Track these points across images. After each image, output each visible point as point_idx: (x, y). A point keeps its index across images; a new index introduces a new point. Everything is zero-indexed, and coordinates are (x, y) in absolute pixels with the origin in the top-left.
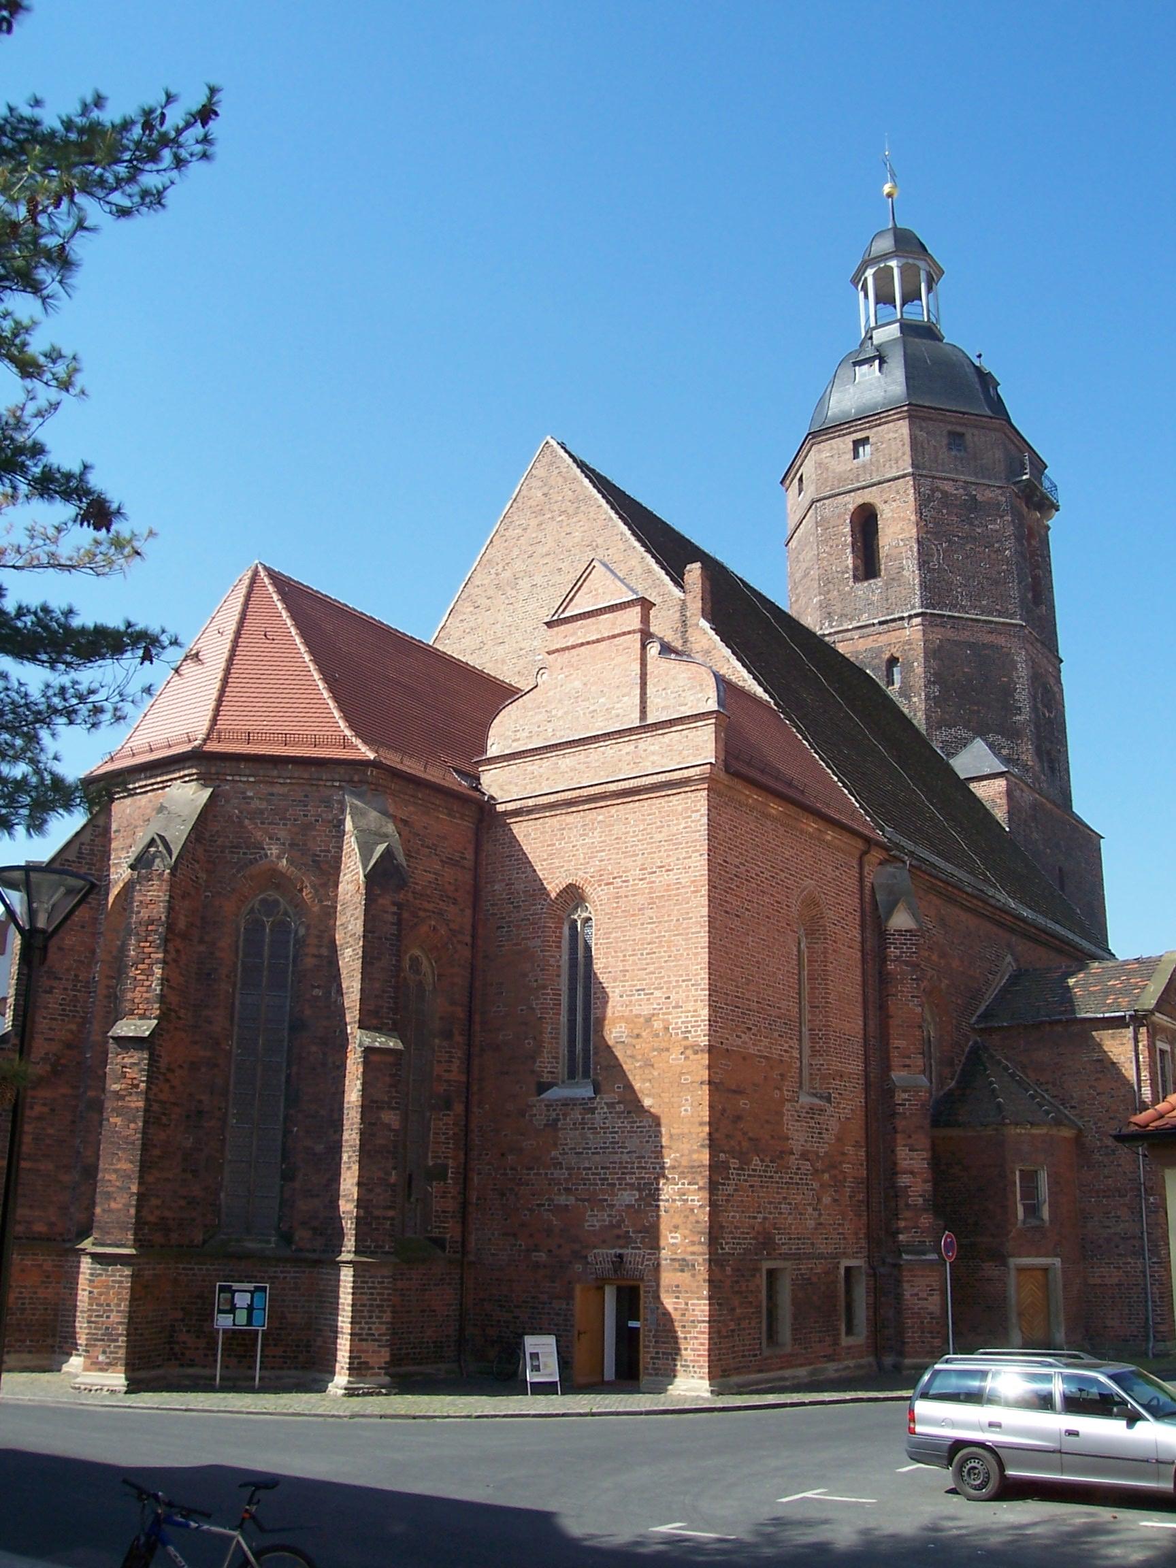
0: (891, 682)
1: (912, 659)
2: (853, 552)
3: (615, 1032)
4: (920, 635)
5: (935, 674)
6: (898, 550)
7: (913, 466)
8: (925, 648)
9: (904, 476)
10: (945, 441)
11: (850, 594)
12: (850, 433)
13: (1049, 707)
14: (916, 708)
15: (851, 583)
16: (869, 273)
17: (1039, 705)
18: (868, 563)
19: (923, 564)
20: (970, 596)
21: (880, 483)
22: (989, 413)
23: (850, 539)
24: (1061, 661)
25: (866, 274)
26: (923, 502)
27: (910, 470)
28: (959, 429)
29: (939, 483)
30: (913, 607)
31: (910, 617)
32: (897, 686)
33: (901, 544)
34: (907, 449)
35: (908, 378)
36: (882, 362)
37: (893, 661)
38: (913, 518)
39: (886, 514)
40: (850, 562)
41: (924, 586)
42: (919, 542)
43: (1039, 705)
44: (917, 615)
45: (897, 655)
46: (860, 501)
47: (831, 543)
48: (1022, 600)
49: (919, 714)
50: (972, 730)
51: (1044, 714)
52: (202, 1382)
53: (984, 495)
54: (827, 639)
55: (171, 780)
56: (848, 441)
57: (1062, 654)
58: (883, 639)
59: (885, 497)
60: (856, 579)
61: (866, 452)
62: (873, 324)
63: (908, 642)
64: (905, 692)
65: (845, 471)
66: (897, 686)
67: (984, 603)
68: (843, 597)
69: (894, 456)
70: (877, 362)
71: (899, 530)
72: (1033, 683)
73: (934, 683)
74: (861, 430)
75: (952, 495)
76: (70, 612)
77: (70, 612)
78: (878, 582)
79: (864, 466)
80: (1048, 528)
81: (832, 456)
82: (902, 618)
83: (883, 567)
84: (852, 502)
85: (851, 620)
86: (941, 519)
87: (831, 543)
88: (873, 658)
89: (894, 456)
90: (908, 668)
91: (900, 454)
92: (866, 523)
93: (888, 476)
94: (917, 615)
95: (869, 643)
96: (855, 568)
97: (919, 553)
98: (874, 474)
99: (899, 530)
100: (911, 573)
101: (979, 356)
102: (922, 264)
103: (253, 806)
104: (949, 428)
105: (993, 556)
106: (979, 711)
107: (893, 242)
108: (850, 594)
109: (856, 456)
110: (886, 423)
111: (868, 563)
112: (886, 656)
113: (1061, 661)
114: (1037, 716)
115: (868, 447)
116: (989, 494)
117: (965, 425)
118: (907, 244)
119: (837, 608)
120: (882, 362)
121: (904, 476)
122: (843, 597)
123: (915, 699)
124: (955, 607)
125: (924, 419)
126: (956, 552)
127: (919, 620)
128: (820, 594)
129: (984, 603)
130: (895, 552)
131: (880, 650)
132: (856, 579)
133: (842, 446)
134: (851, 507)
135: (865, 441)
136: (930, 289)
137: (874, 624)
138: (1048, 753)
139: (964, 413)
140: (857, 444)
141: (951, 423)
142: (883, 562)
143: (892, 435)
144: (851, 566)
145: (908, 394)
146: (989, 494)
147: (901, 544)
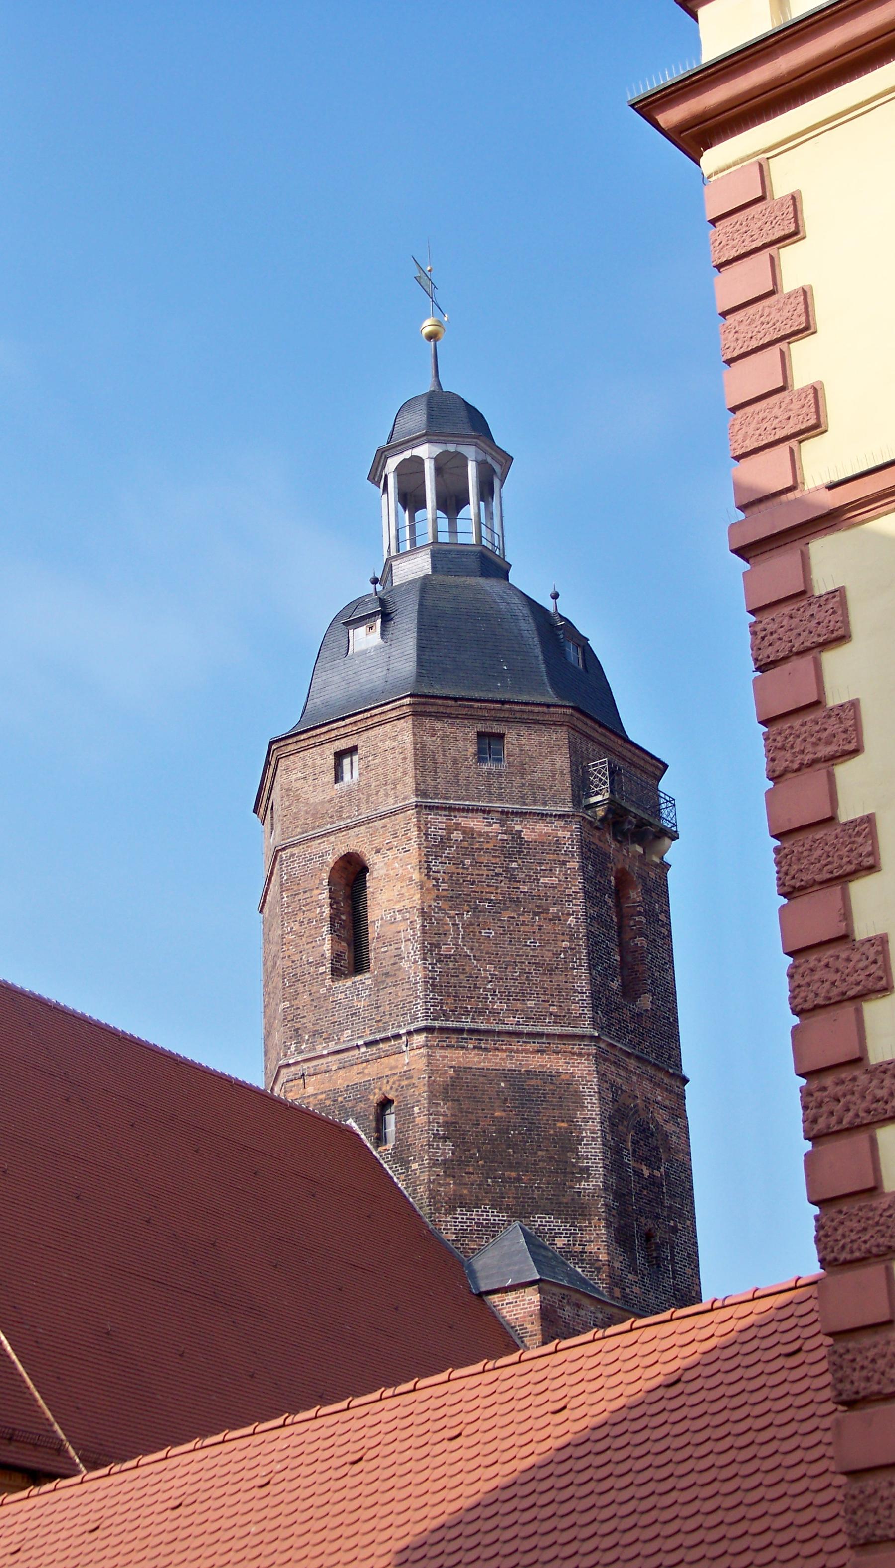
0: (380, 1139)
1: (411, 1101)
2: (333, 930)
4: (421, 1064)
5: (446, 1124)
6: (394, 928)
7: (419, 792)
8: (430, 1085)
9: (404, 809)
10: (472, 749)
11: (326, 998)
12: (330, 740)
13: (653, 1161)
14: (416, 1180)
15: (328, 982)
16: (392, 463)
17: (629, 1160)
19: (431, 948)
20: (508, 996)
21: (370, 820)
22: (555, 700)
23: (327, 911)
24: (685, 1081)
25: (386, 471)
26: (434, 848)
27: (413, 799)
28: (496, 728)
30: (414, 1019)
31: (409, 1033)
32: (390, 1146)
33: (399, 917)
34: (410, 766)
35: (421, 648)
36: (386, 617)
37: (385, 1104)
38: (416, 876)
41: (432, 984)
42: (423, 914)
43: (629, 1160)
44: (418, 1031)
45: (390, 1096)
46: (342, 850)
47: (300, 917)
48: (595, 996)
49: (421, 1189)
50: (508, 1209)
51: (639, 1174)
55: (268, 799)
56: (324, 757)
57: (686, 1071)
58: (372, 1070)
59: (377, 843)
60: (337, 973)
61: (352, 771)
62: (393, 553)
64: (401, 1158)
65: (322, 802)
66: (390, 1146)
67: (530, 1004)
68: (317, 1002)
69: (391, 777)
70: (379, 622)
72: (612, 1125)
73: (444, 1138)
74: (346, 735)
75: (480, 834)
78: (366, 978)
79: (349, 793)
80: (666, 866)
81: (306, 777)
82: (398, 1036)
83: (372, 955)
84: (332, 850)
85: (327, 1039)
87: (300, 917)
88: (357, 1101)
89: (391, 777)
90: (405, 1117)
91: (399, 774)
93: (383, 809)
94: (418, 1031)
95: (352, 1077)
96: (337, 957)
97: (424, 932)
98: (364, 806)
99: (395, 897)
100: (413, 967)
101: (555, 596)
102: (470, 452)
103: (348, 1122)
104: (480, 727)
105: (548, 927)
106: (518, 1179)
107: (425, 417)
108: (326, 998)
109: (338, 778)
110: (381, 724)
112: (375, 1098)
113: (685, 1081)
114: (623, 1179)
115: (355, 758)
116: (542, 828)
117: (506, 720)
118: (453, 417)
119: (308, 1021)
120: (386, 617)
121: (404, 809)
122: (317, 1002)
123: (415, 1166)
124: (481, 1013)
125: (439, 716)
126: (485, 926)
127: (419, 1039)
128: (285, 1000)
129: (530, 1004)
130: (389, 931)
131: (366, 1087)
132: (337, 973)
133: (319, 762)
134: (331, 859)
135: (353, 750)
136: (487, 492)
137: (358, 1047)
138: (648, 1236)
139: (503, 703)
140: (339, 756)
141: (480, 718)
142: (372, 946)
143: (389, 744)
144: (328, 954)
145: (419, 675)
147: (399, 917)
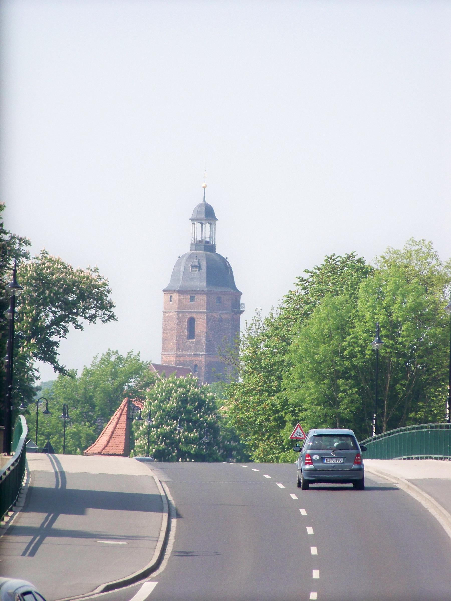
3: (242, 301)
18: (191, 335)
19: (207, 337)
29: (213, 314)
34: (206, 304)
39: (198, 322)
40: (186, 333)
46: (191, 316)
52: (131, 414)
53: (224, 316)
54: (11, 524)
63: (201, 361)
71: (201, 326)
76: (109, 292)
77: (109, 292)
84: (189, 315)
86: (214, 326)
92: (192, 321)
99: (201, 326)
111: (191, 335)
112: (194, 364)
134: (188, 316)
146: (226, 316)
